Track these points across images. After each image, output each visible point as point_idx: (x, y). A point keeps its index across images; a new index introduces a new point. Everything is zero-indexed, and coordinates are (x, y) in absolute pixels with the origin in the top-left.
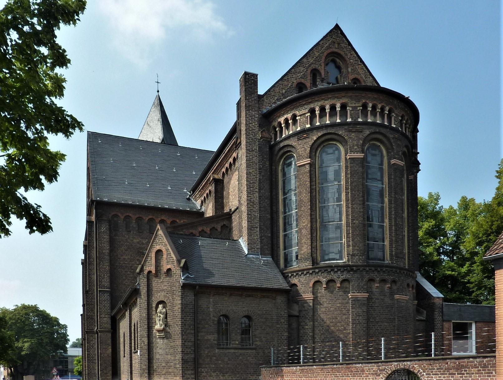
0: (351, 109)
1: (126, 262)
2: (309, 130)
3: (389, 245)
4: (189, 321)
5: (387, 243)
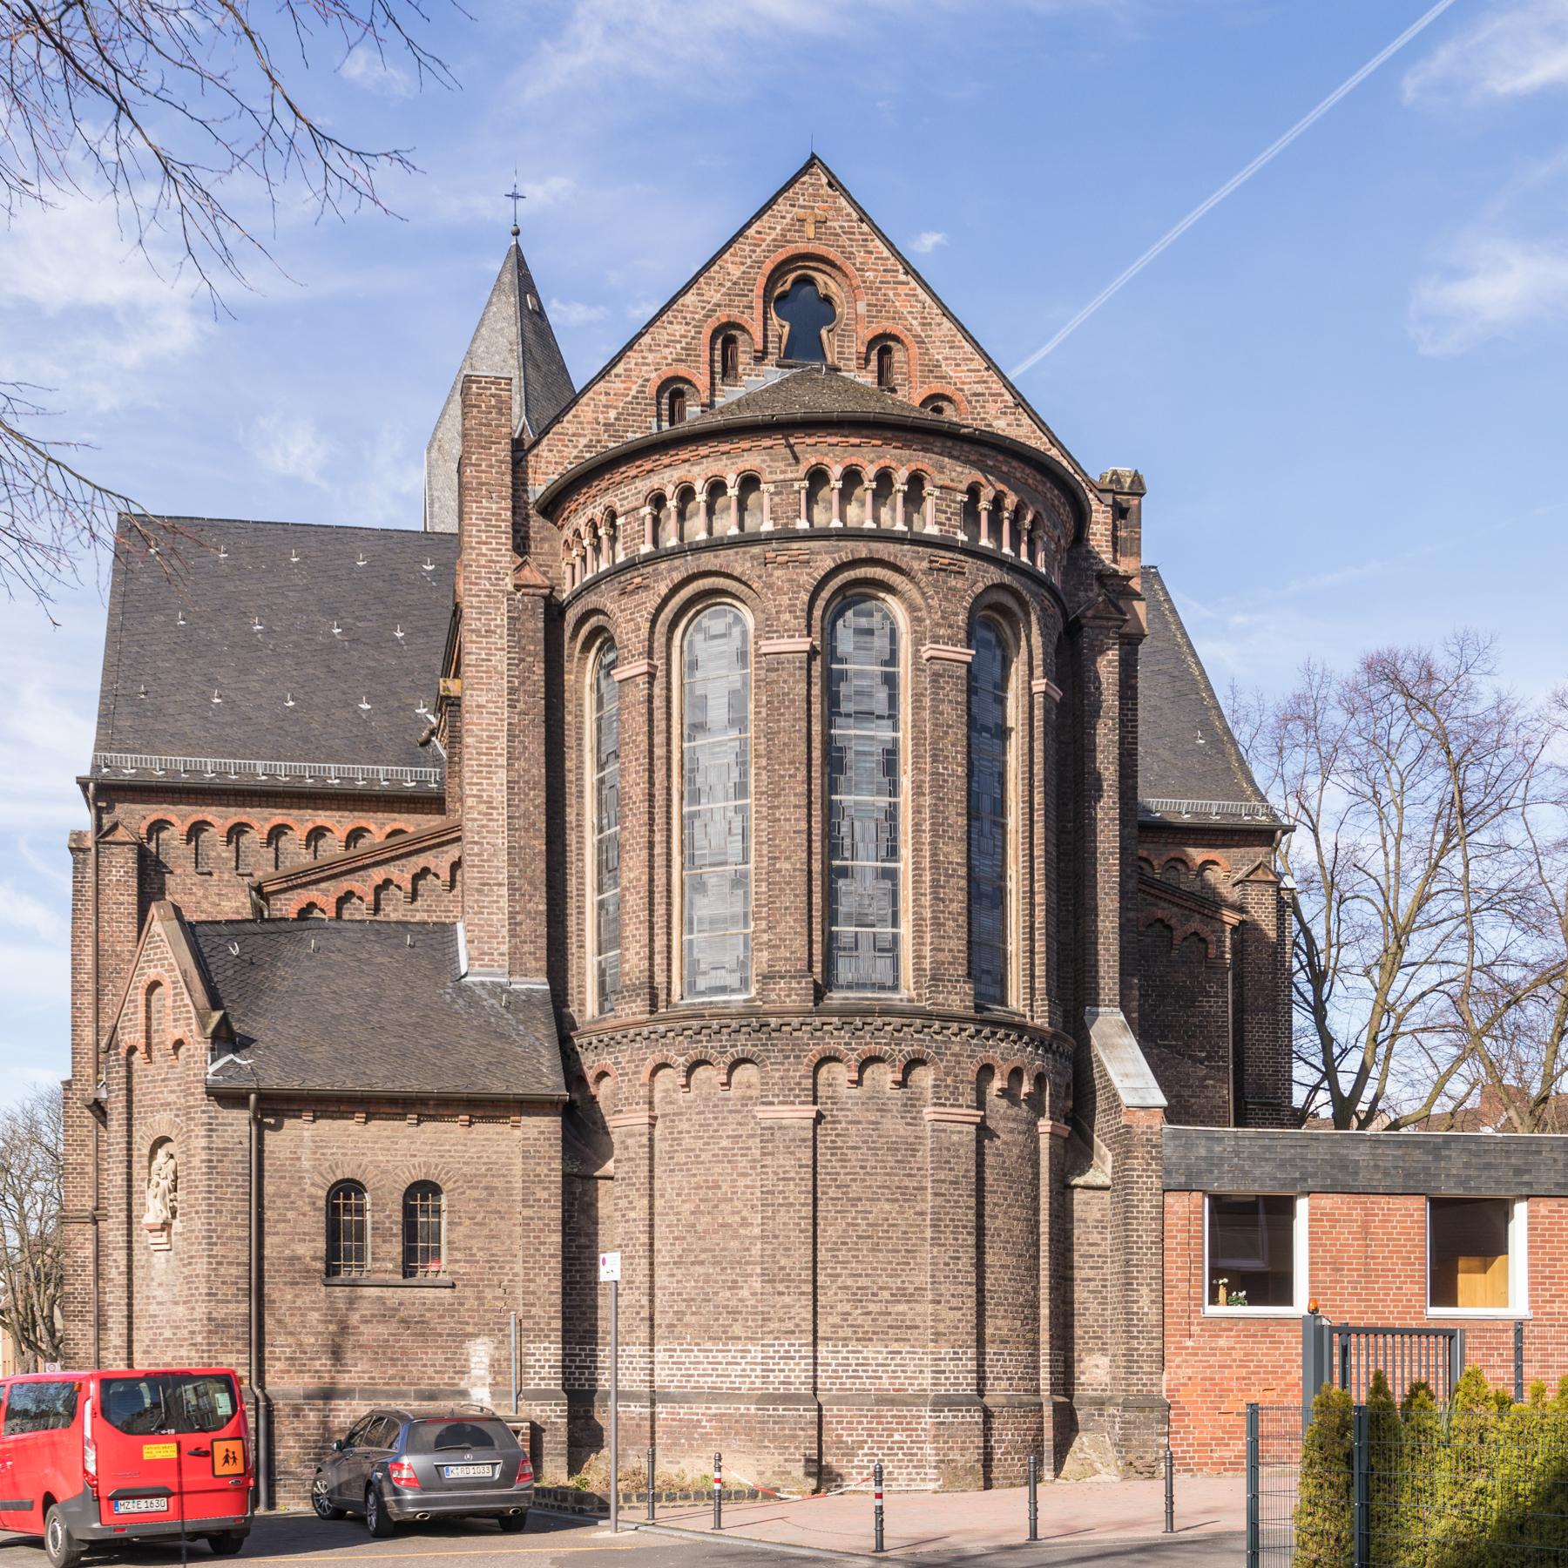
0: (772, 489)
2: (649, 560)
3: (911, 936)
4: (231, 1200)
5: (906, 930)
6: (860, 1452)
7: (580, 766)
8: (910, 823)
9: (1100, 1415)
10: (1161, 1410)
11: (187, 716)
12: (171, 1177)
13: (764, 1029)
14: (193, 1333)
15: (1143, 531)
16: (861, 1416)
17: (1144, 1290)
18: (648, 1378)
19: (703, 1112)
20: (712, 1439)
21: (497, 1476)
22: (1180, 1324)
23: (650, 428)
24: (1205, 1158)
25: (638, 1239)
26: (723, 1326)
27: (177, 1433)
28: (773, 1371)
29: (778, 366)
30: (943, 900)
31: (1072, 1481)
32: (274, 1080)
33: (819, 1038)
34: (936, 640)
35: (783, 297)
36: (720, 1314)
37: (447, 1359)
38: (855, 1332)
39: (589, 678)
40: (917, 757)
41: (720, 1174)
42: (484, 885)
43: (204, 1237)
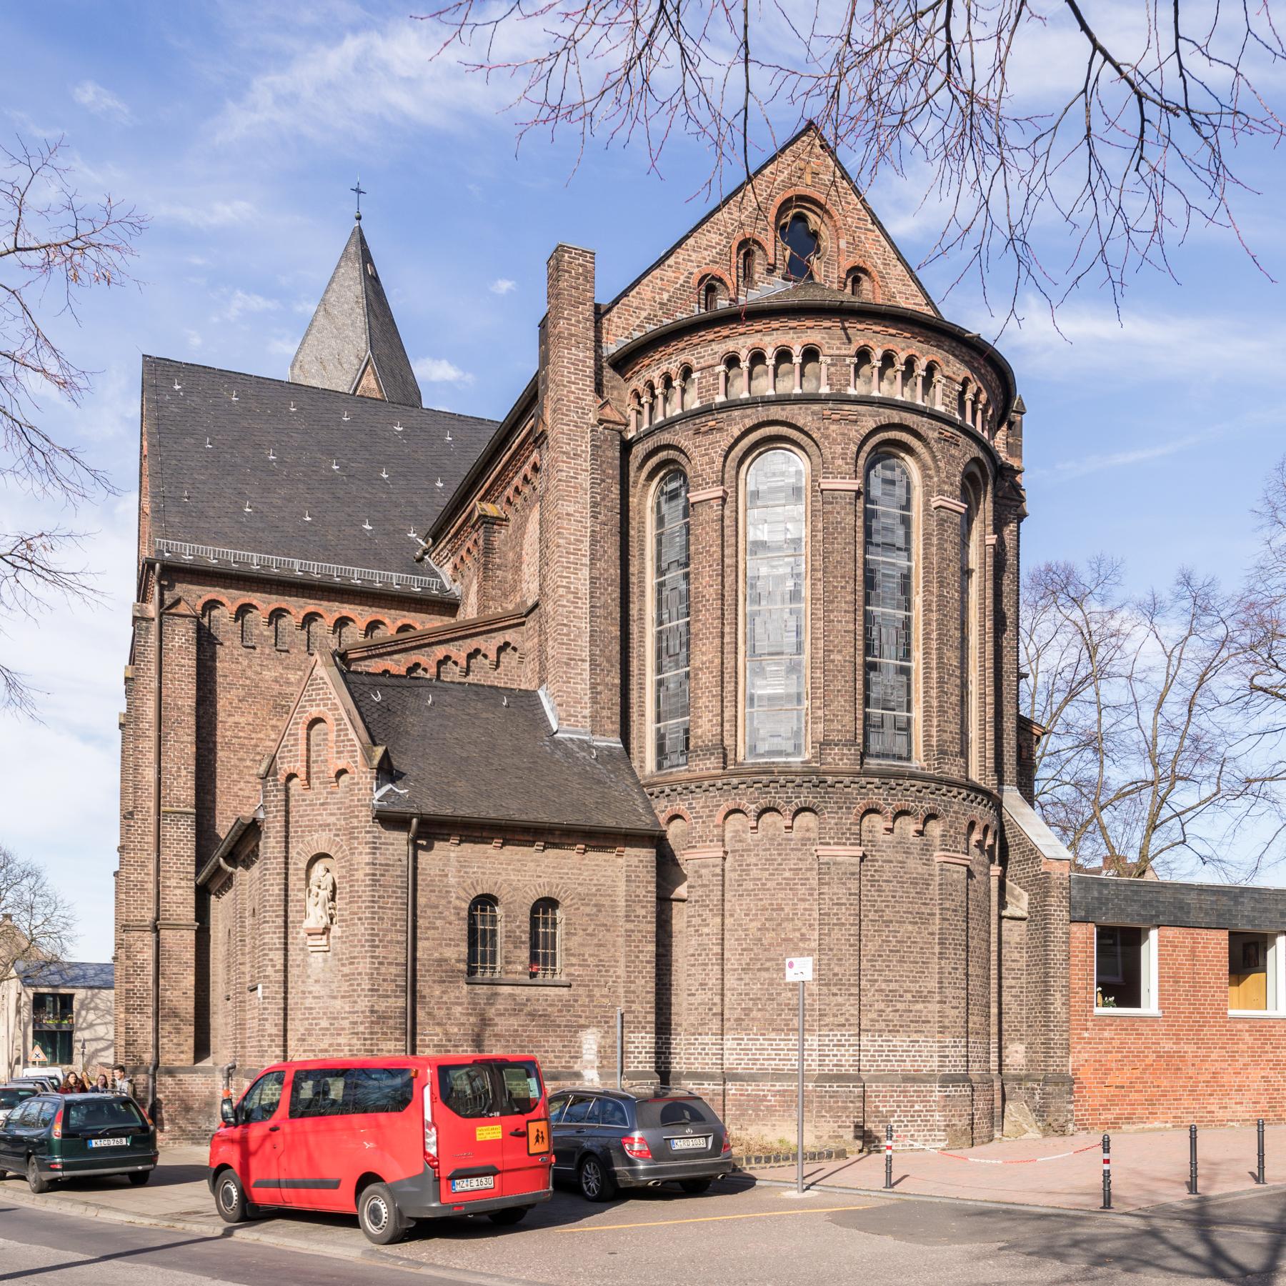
0: (829, 361)
1: (241, 734)
4: (391, 909)
5: (917, 714)
6: (892, 1119)
7: (642, 571)
8: (921, 632)
9: (1020, 1088)
10: (1067, 1082)
11: (226, 520)
12: (330, 888)
13: (821, 785)
14: (355, 1023)
15: (1024, 439)
16: (892, 1091)
17: (1058, 995)
18: (720, 1062)
19: (769, 849)
20: (776, 1111)
21: (710, 1147)
22: (1080, 1020)
23: (693, 311)
24: (1097, 898)
25: (712, 949)
26: (785, 1020)
27: (501, 1115)
28: (828, 1056)
29: (784, 278)
30: (946, 693)
31: (1013, 1138)
32: (430, 807)
33: (864, 794)
34: (941, 492)
35: (784, 226)
36: (783, 1010)
37: (564, 1046)
38: (888, 1025)
39: (650, 502)
40: (927, 582)
41: (782, 899)
42: (571, 659)
43: (367, 941)
